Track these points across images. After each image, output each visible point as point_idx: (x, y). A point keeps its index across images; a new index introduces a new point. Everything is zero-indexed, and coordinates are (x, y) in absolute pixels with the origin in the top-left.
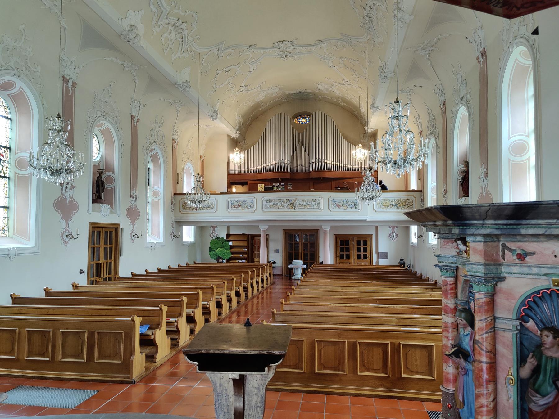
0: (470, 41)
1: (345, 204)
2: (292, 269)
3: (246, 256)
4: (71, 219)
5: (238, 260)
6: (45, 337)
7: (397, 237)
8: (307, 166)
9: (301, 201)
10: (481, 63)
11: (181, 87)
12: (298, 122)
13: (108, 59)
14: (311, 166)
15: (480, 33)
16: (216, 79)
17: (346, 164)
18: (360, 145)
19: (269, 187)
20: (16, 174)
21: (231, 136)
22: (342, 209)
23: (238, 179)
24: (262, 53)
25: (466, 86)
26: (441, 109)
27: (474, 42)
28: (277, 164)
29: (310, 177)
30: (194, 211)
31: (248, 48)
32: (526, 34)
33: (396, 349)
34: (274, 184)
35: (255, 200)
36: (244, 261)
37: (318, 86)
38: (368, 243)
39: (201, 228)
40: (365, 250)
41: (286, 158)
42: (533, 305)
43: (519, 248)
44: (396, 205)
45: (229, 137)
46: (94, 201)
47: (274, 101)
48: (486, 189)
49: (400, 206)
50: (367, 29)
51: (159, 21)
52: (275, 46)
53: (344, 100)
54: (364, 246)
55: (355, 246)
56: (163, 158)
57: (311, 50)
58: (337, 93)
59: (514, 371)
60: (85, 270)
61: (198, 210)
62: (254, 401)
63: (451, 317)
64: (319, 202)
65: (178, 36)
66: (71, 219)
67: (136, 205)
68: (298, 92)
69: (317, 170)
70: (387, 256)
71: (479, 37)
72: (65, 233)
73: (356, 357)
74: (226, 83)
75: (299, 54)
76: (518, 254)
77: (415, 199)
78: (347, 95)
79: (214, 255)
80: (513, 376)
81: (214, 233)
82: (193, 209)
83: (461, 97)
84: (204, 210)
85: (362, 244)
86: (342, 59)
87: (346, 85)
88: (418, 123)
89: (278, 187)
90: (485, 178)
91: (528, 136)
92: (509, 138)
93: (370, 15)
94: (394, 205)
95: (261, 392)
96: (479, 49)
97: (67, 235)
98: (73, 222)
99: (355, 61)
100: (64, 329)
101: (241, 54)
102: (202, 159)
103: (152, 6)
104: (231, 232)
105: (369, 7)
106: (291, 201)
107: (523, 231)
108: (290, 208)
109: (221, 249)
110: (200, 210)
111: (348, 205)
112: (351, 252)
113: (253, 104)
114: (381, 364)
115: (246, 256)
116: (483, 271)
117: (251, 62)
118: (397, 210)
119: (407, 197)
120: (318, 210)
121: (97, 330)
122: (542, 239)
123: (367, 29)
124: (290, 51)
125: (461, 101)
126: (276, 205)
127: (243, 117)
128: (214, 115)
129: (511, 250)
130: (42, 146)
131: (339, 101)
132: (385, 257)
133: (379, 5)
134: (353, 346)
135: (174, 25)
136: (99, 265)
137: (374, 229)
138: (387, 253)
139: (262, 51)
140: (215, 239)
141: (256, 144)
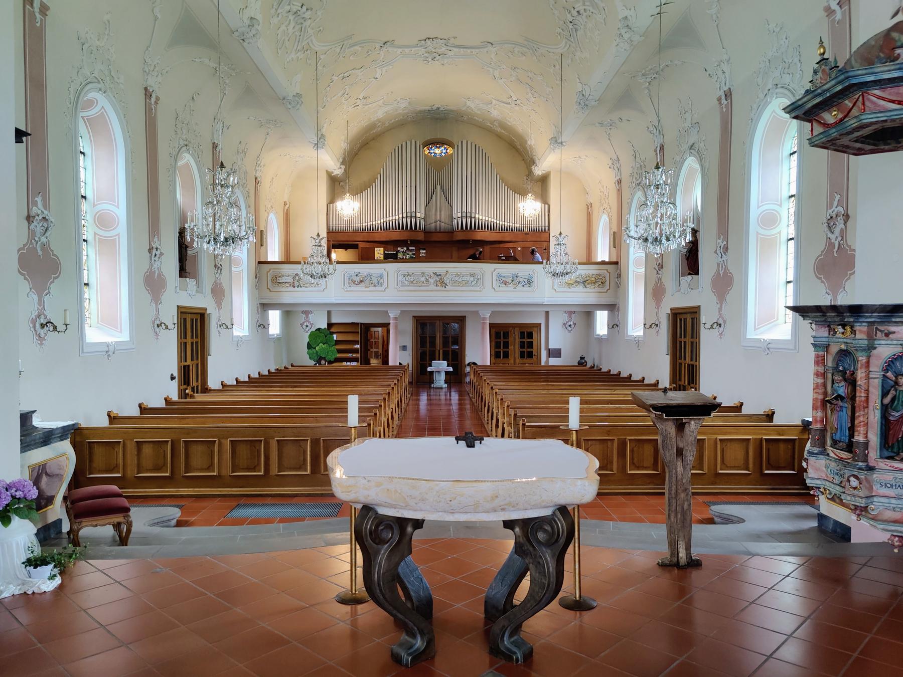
0: (709, 75)
1: (514, 281)
2: (432, 373)
3: (358, 355)
4: (47, 291)
5: (345, 362)
6: (255, 448)
8: (450, 223)
9: (454, 276)
11: (290, 103)
12: (429, 153)
13: (199, 60)
14: (455, 222)
15: (725, 67)
16: (328, 88)
17: (506, 221)
18: (530, 195)
19: (392, 252)
20: (97, 236)
21: (333, 172)
23: (343, 239)
24: (399, 52)
25: (698, 131)
26: (657, 154)
28: (405, 218)
29: (454, 239)
30: (291, 289)
31: (382, 45)
32: (791, 85)
35: (385, 274)
36: (355, 363)
37: (467, 102)
38: (535, 336)
39: (288, 313)
40: (531, 345)
41: (418, 210)
42: (891, 364)
43: (885, 329)
44: (584, 282)
46: (181, 276)
47: (397, 120)
48: (724, 267)
49: (588, 284)
50: (566, 38)
52: (421, 44)
53: (502, 125)
54: (529, 340)
55: (516, 340)
56: (246, 205)
57: (472, 54)
58: (495, 114)
59: (879, 401)
60: (176, 374)
61: (296, 288)
62: (690, 440)
63: (821, 379)
64: (479, 277)
65: (298, 27)
66: (47, 291)
67: (220, 279)
68: (435, 108)
69: (469, 229)
70: (560, 353)
71: (724, 72)
74: (340, 94)
75: (452, 58)
76: (885, 333)
77: (608, 274)
78: (510, 119)
79: (314, 355)
80: (878, 405)
81: (307, 321)
82: (289, 285)
83: (690, 143)
86: (516, 70)
87: (513, 105)
88: (615, 167)
89: (406, 252)
90: (724, 253)
91: (780, 205)
93: (576, 22)
94: (581, 283)
97: (158, 325)
98: (51, 297)
99: (535, 76)
100: (280, 438)
101: (370, 52)
102: (287, 207)
104: (334, 321)
106: (440, 275)
107: (894, 320)
109: (323, 346)
112: (511, 348)
114: (651, 460)
115: (358, 355)
116: (867, 343)
117: (381, 64)
118: (585, 290)
119: (598, 271)
120: (478, 289)
122: (900, 324)
123: (566, 38)
124: (440, 53)
125: (691, 149)
128: (319, 142)
129: (881, 331)
131: (493, 125)
132: (559, 355)
133: (592, 13)
134: (622, 444)
135: (296, 13)
136: (187, 369)
138: (560, 350)
139: (400, 50)
140: (316, 330)
141: (371, 186)
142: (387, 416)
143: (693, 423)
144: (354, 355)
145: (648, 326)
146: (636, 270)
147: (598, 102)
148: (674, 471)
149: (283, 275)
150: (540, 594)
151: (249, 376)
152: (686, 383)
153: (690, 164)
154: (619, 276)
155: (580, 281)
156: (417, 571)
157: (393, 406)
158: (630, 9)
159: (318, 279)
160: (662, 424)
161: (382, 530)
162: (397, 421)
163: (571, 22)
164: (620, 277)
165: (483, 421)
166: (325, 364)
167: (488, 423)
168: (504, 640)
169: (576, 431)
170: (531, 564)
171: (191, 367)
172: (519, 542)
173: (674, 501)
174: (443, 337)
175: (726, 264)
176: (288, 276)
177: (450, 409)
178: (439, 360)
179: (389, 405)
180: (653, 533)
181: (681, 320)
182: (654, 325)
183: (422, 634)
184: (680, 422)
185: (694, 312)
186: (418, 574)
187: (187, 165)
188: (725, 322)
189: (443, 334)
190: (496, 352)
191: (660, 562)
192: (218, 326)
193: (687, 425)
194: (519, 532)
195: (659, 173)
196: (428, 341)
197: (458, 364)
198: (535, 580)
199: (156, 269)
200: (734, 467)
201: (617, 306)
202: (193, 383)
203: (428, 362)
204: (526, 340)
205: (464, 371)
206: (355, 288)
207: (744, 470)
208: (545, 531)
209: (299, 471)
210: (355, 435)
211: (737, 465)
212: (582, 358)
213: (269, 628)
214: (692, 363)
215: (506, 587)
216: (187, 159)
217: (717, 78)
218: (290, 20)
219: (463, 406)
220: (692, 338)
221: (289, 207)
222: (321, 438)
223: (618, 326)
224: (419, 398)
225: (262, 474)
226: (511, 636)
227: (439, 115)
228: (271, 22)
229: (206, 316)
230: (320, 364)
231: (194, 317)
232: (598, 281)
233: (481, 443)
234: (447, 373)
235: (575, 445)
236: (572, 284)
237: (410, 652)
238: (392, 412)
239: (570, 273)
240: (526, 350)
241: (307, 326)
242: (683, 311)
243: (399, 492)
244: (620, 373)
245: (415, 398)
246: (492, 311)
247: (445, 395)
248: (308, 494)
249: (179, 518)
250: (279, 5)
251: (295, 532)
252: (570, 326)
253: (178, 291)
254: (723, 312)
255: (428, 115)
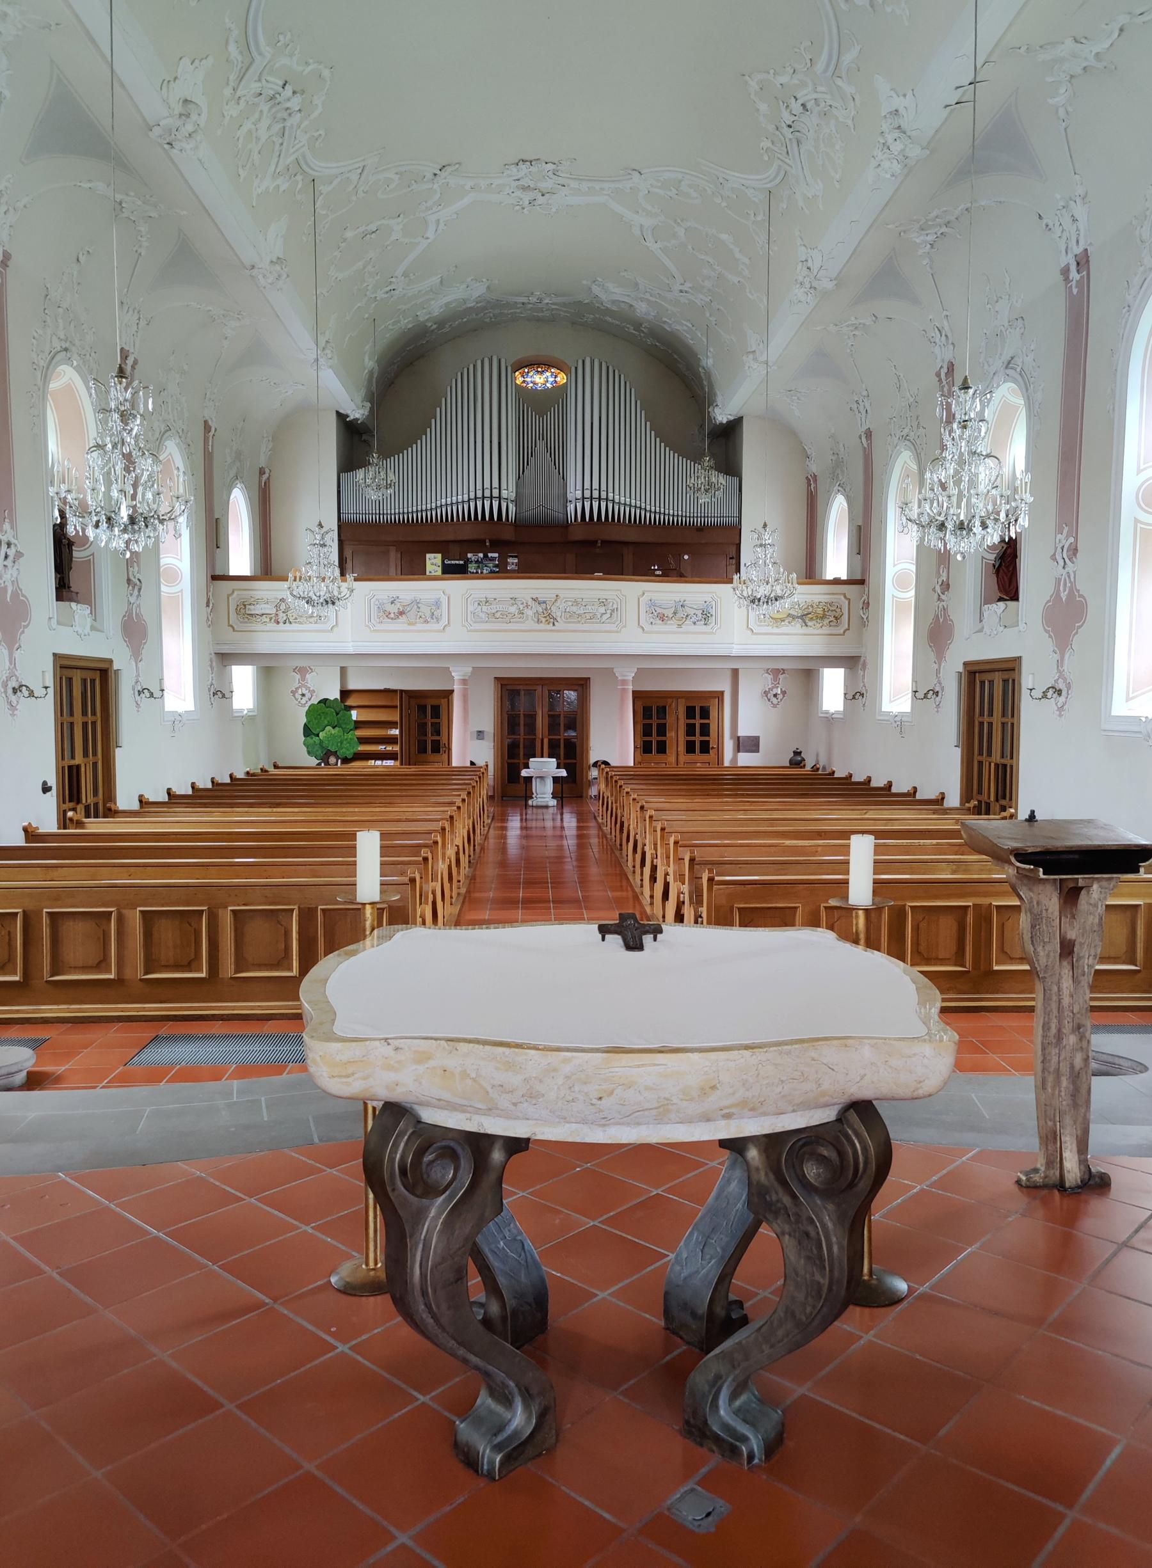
0: (1047, 226)
1: (678, 614)
2: (529, 780)
3: (397, 748)
4: (18, 645)
5: (372, 759)
6: (190, 925)
7: (784, 696)
10: (1074, 283)
11: (264, 276)
15: (1079, 211)
19: (457, 562)
21: (347, 416)
22: (672, 624)
27: (1058, 231)
30: (272, 626)
31: (438, 172)
33: (984, 915)
34: (469, 555)
36: (390, 763)
38: (713, 714)
40: (705, 730)
41: (504, 486)
44: (803, 617)
45: (341, 417)
46: (59, 598)
47: (465, 320)
48: (1068, 585)
49: (811, 619)
51: (240, 88)
60: (52, 782)
61: (281, 624)
64: (615, 606)
65: (277, 127)
66: (18, 645)
67: (139, 606)
71: (1075, 220)
72: (9, 683)
73: (905, 937)
77: (847, 602)
79: (316, 748)
82: (268, 620)
83: (1006, 357)
84: (300, 623)
85: (698, 716)
89: (481, 562)
92: (1139, 472)
94: (798, 617)
95: (1099, 911)
96: (1072, 249)
97: (14, 689)
100: (239, 905)
102: (265, 477)
103: (232, 48)
104: (351, 686)
105: (802, 105)
106: (544, 602)
108: (541, 622)
109: (333, 731)
110: (287, 624)
111: (687, 616)
112: (671, 734)
113: (410, 326)
114: (953, 947)
118: (805, 630)
120: (612, 627)
121: (323, 905)
125: (1006, 368)
126: (505, 614)
127: (378, 362)
130: (87, 453)
133: (831, 106)
135: (272, 98)
136: (75, 771)
137: (729, 675)
140: (320, 702)
142: (447, 861)
143: (1095, 886)
144: (389, 748)
145: (920, 695)
146: (897, 594)
147: (835, 282)
148: (1055, 988)
149: (258, 602)
150: (809, 1309)
151: (193, 785)
152: (992, 798)
153: (1004, 396)
154: (866, 605)
155: (796, 614)
156: (512, 1225)
157: (458, 841)
158: (905, 96)
159: (320, 607)
160: (1030, 890)
161: (431, 1162)
162: (467, 868)
163: (790, 126)
164: (868, 608)
165: (625, 868)
166: (337, 764)
167: (634, 872)
168: (717, 1407)
169: (866, 911)
170: (787, 1237)
171: (83, 769)
172: (758, 1182)
173: (1055, 1051)
174: (549, 716)
175: (1072, 580)
176: (267, 603)
177: (562, 846)
178: (542, 757)
179: (452, 840)
180: (973, 1095)
181: (982, 683)
182: (931, 692)
183: (527, 1396)
184: (1072, 885)
185: (1009, 669)
186: (514, 1231)
187: (69, 389)
188: (1069, 686)
189: (549, 711)
190: (644, 742)
191: (1024, 1178)
192: (134, 694)
193: (1083, 892)
194: (757, 1158)
195: (968, 399)
196: (522, 723)
197: (576, 763)
198: (797, 1274)
199: (9, 584)
200: (1109, 958)
201: (862, 659)
202: (87, 797)
203: (522, 761)
204: (698, 722)
205: (587, 778)
206: (389, 625)
207: (1124, 963)
208: (822, 1160)
209: (277, 970)
210: (373, 920)
211: (1113, 955)
212: (797, 753)
213: (175, 1365)
214: (1003, 761)
215: (713, 1261)
216: (66, 377)
217: (1062, 232)
218: (261, 111)
219: (584, 841)
220: (1003, 716)
221: (268, 478)
222: (319, 907)
223: (862, 695)
224: (505, 825)
225: (203, 975)
226: (734, 1396)
227: (542, 311)
228: (225, 113)
229: (112, 675)
230: (327, 763)
231: (89, 675)
232: (828, 615)
233: (655, 939)
234: (556, 780)
235: (862, 941)
236: (783, 620)
237: (499, 1438)
238: (457, 853)
239: (782, 597)
240: (698, 738)
241: (303, 695)
242: (988, 667)
243: (473, 1075)
244: (869, 780)
245: (500, 825)
246: (638, 669)
247: (553, 819)
248: (292, 1014)
249: (33, 1066)
250: (241, 81)
251: (263, 1099)
252: (775, 695)
253: (54, 627)
254: (1065, 667)
255: (522, 313)
